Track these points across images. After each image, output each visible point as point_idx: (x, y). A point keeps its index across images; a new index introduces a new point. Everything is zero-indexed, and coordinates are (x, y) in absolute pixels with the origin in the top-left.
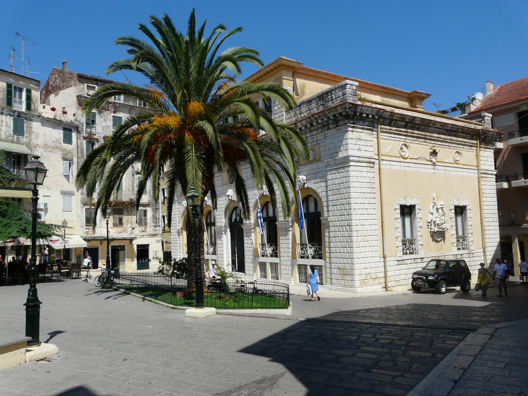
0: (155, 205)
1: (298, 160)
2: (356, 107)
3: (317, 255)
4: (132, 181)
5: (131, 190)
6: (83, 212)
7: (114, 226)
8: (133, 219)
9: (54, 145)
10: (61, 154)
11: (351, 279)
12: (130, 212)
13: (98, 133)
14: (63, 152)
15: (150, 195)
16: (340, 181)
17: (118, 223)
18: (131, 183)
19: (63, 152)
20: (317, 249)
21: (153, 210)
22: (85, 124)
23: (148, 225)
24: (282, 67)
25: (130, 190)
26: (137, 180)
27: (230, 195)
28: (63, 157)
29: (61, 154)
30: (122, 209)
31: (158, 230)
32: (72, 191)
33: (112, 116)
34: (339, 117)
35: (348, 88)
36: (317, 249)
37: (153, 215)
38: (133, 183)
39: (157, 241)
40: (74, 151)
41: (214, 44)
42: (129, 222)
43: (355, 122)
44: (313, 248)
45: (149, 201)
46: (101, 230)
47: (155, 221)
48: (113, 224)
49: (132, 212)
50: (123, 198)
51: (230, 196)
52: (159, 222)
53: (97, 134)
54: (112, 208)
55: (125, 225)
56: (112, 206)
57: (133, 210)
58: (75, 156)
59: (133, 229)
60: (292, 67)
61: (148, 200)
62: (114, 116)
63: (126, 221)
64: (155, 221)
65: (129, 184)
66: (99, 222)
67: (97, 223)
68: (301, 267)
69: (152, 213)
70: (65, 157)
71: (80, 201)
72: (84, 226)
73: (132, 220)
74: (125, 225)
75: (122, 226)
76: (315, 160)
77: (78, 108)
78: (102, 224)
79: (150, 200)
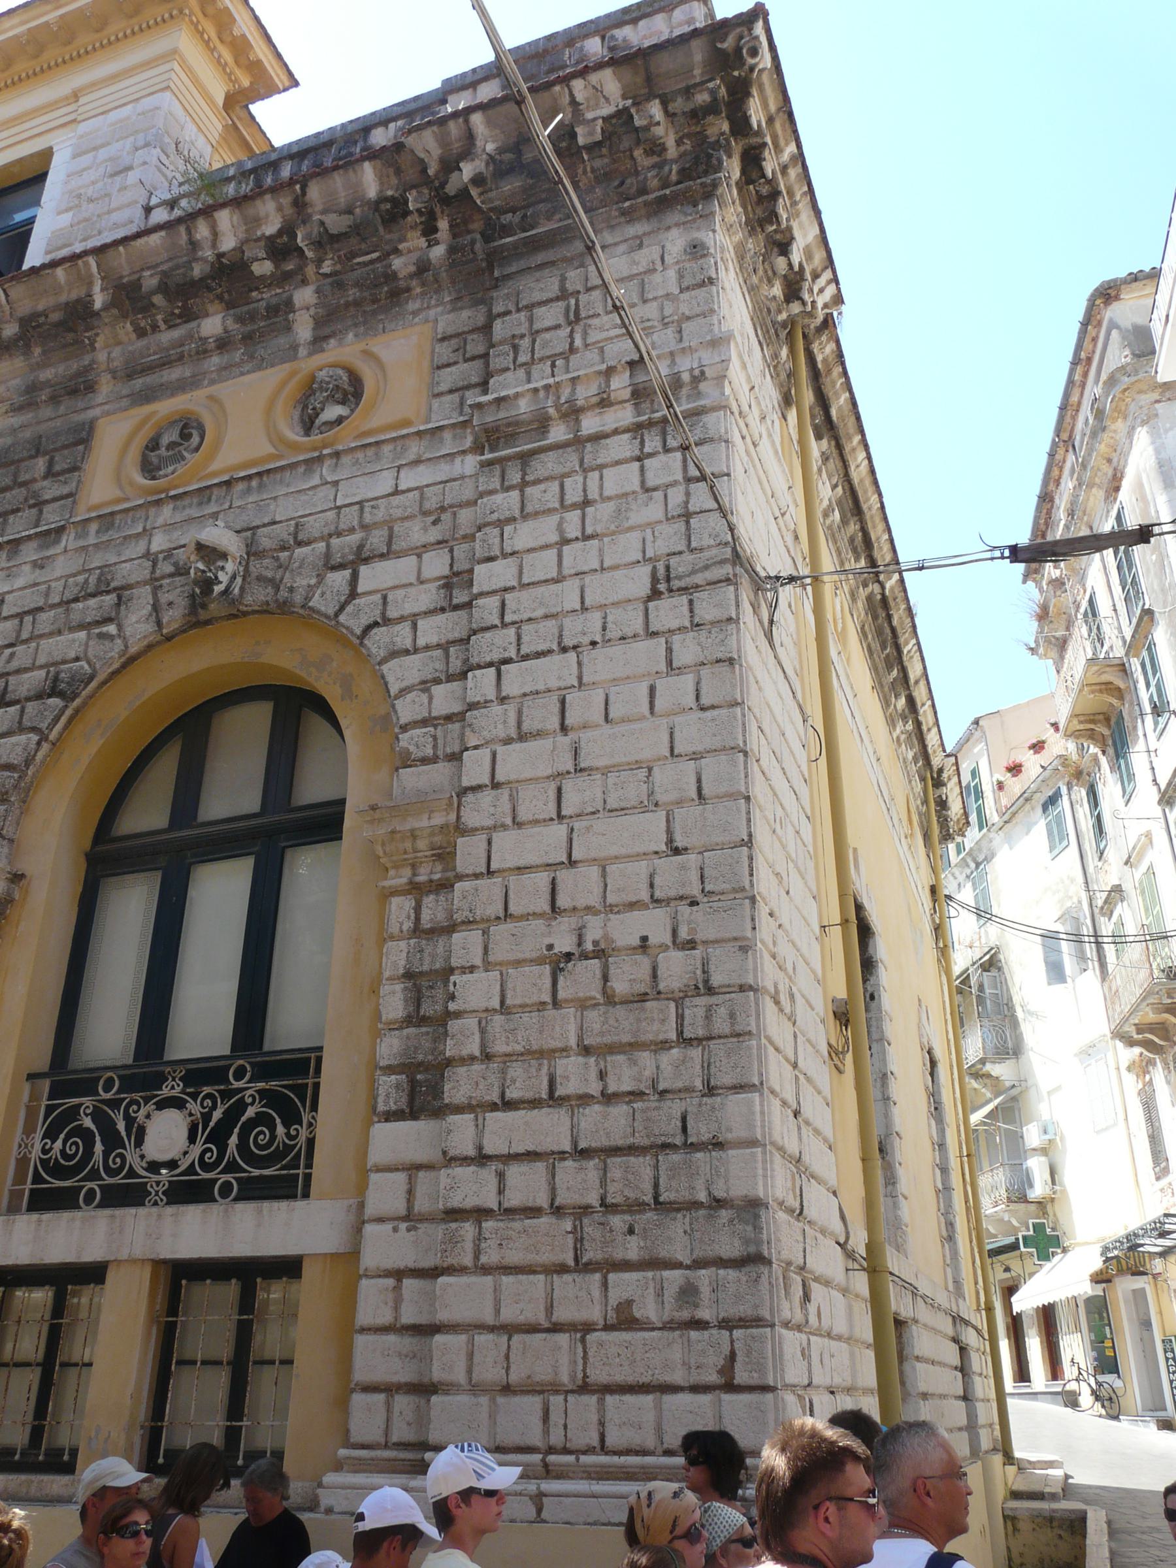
3: (232, 1167)
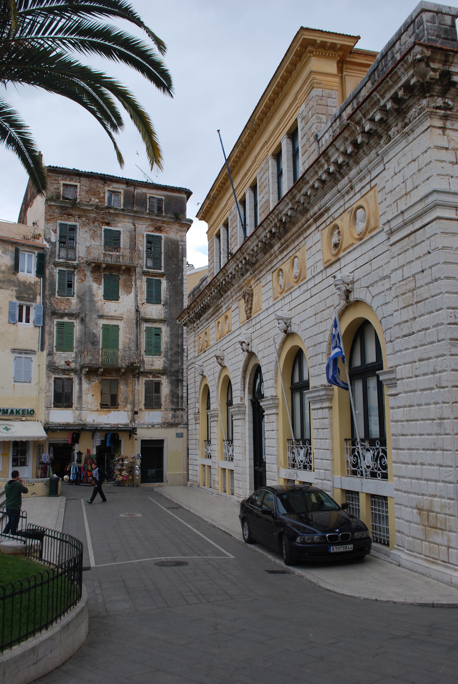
0: (176, 374)
1: (339, 241)
2: (447, 56)
3: (379, 470)
4: (135, 333)
5: (133, 349)
6: (50, 385)
7: (101, 408)
8: (136, 397)
9: (4, 277)
10: (15, 290)
11: (446, 543)
12: (131, 385)
13: (79, 257)
14: (17, 288)
15: (166, 356)
16: (416, 267)
17: (109, 403)
18: (133, 337)
19: (17, 288)
20: (378, 453)
21: (171, 383)
22: (58, 243)
23: (162, 407)
24: (310, 48)
25: (132, 348)
26: (144, 332)
27: (244, 342)
28: (18, 295)
29: (15, 290)
30: (117, 380)
31: (180, 417)
32: (32, 349)
33: (103, 230)
34: (406, 97)
35: (427, 21)
36: (378, 453)
37: (171, 391)
38: (137, 337)
39: (177, 434)
40: (38, 286)
41: (448, 221)
42: (129, 402)
43: (450, 103)
44: (371, 451)
45: (166, 367)
46: (81, 413)
47: (175, 400)
48: (100, 404)
49: (135, 385)
50: (119, 361)
51: (244, 344)
52: (182, 403)
53: (77, 259)
54: (99, 378)
55: (122, 406)
56: (100, 375)
57: (137, 382)
58: (40, 295)
59: (136, 413)
60: (333, 47)
61: (162, 365)
62: (106, 230)
63: (123, 399)
64: (175, 400)
65: (130, 339)
66: (76, 400)
67: (73, 402)
68: (352, 497)
69: (169, 388)
70: (22, 295)
71: (45, 366)
72: (51, 407)
73: (134, 398)
74: (122, 406)
75: (117, 408)
76: (369, 229)
77: (48, 220)
78: (81, 404)
79: (166, 365)
